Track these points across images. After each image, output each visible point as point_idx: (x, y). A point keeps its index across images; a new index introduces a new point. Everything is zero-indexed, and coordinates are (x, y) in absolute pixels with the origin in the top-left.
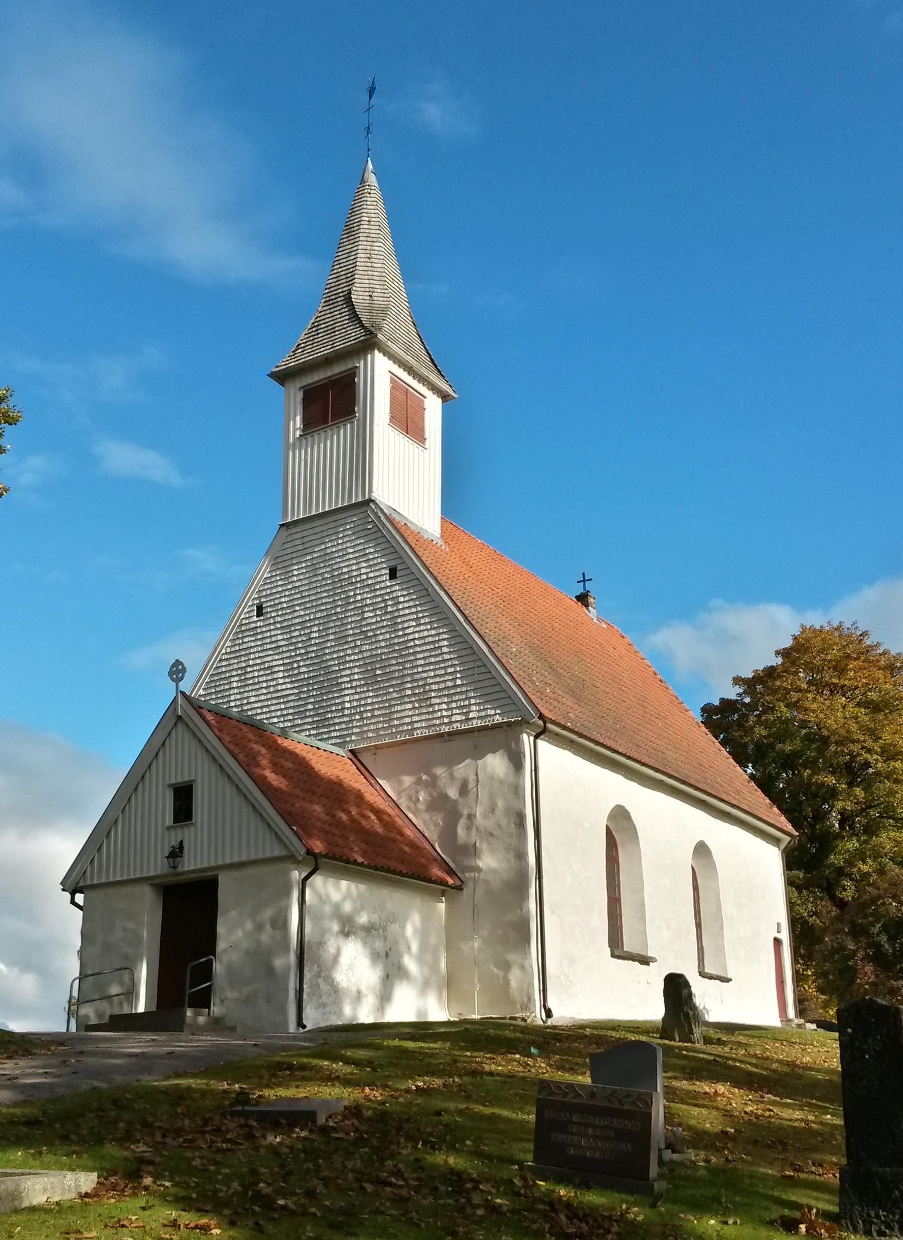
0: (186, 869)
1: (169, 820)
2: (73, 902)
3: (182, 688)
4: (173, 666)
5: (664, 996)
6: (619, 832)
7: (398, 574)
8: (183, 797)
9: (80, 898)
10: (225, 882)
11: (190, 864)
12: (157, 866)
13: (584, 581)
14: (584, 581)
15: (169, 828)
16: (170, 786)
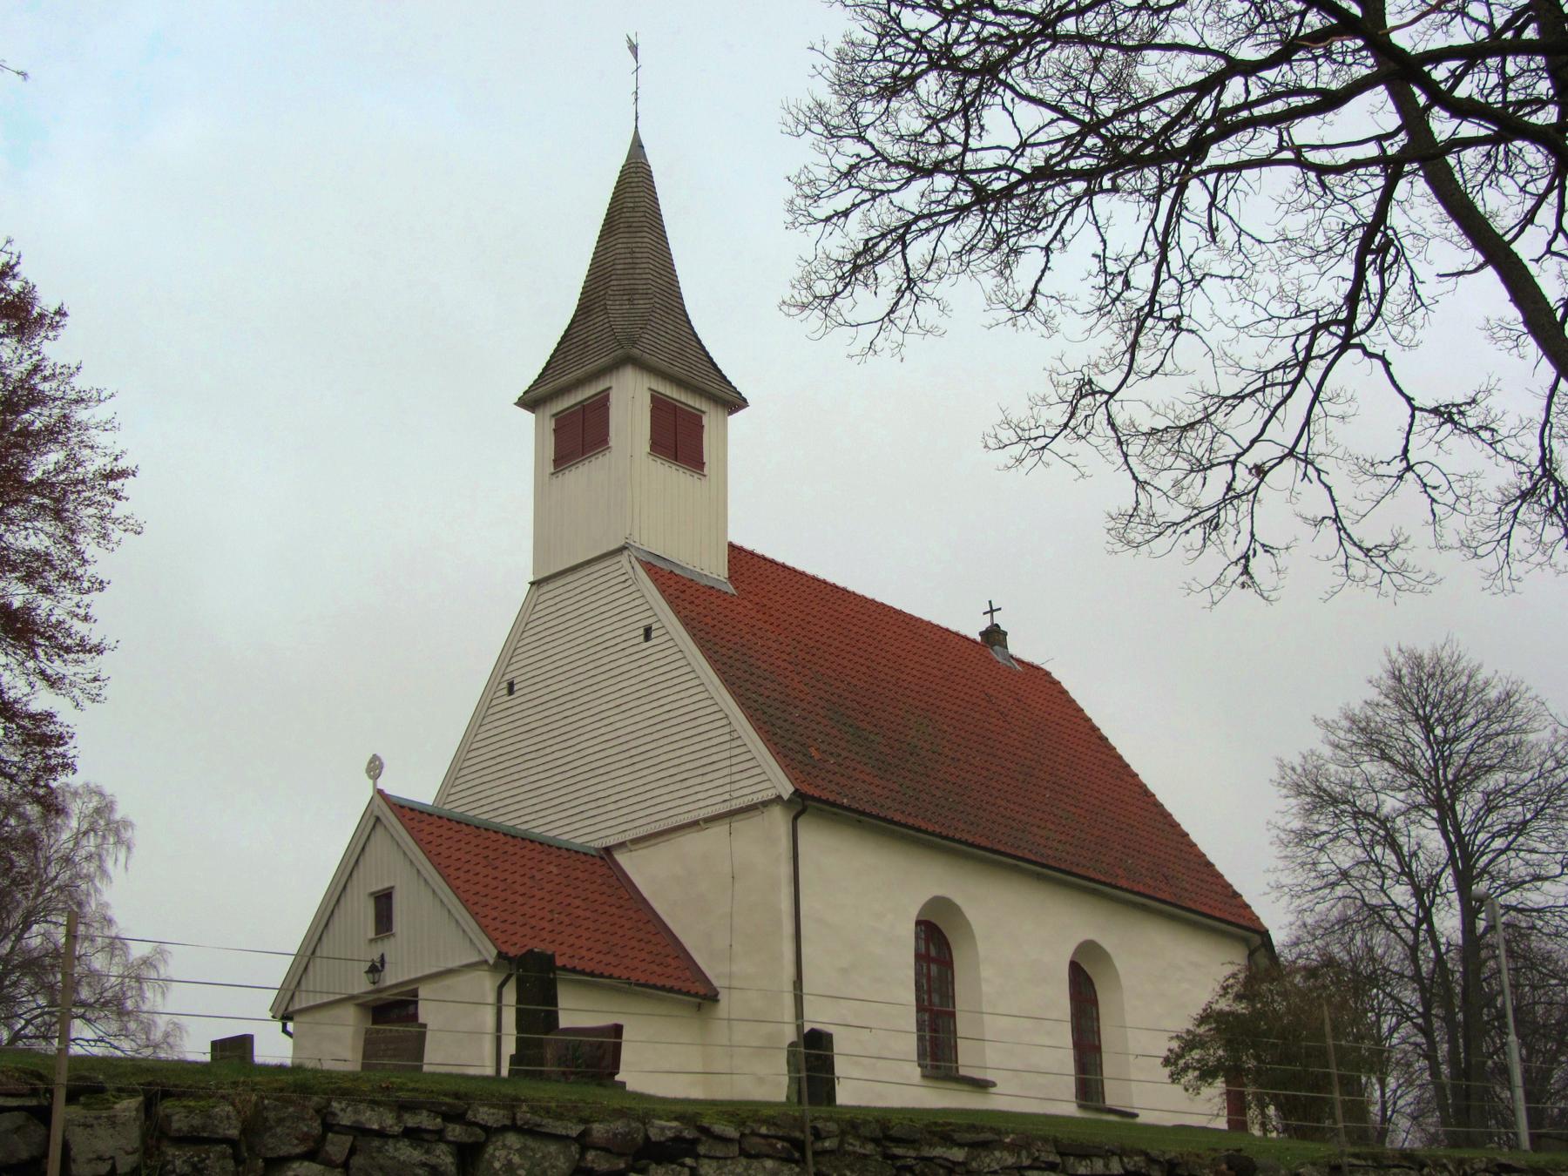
0: (388, 983)
1: (372, 935)
2: (285, 1030)
3: (380, 786)
4: (371, 762)
5: (814, 579)
6: (936, 944)
7: (641, 631)
8: (383, 901)
9: (290, 1026)
10: (424, 992)
11: (391, 977)
12: (361, 985)
13: (992, 611)
14: (992, 611)
15: (371, 941)
16: (372, 894)
